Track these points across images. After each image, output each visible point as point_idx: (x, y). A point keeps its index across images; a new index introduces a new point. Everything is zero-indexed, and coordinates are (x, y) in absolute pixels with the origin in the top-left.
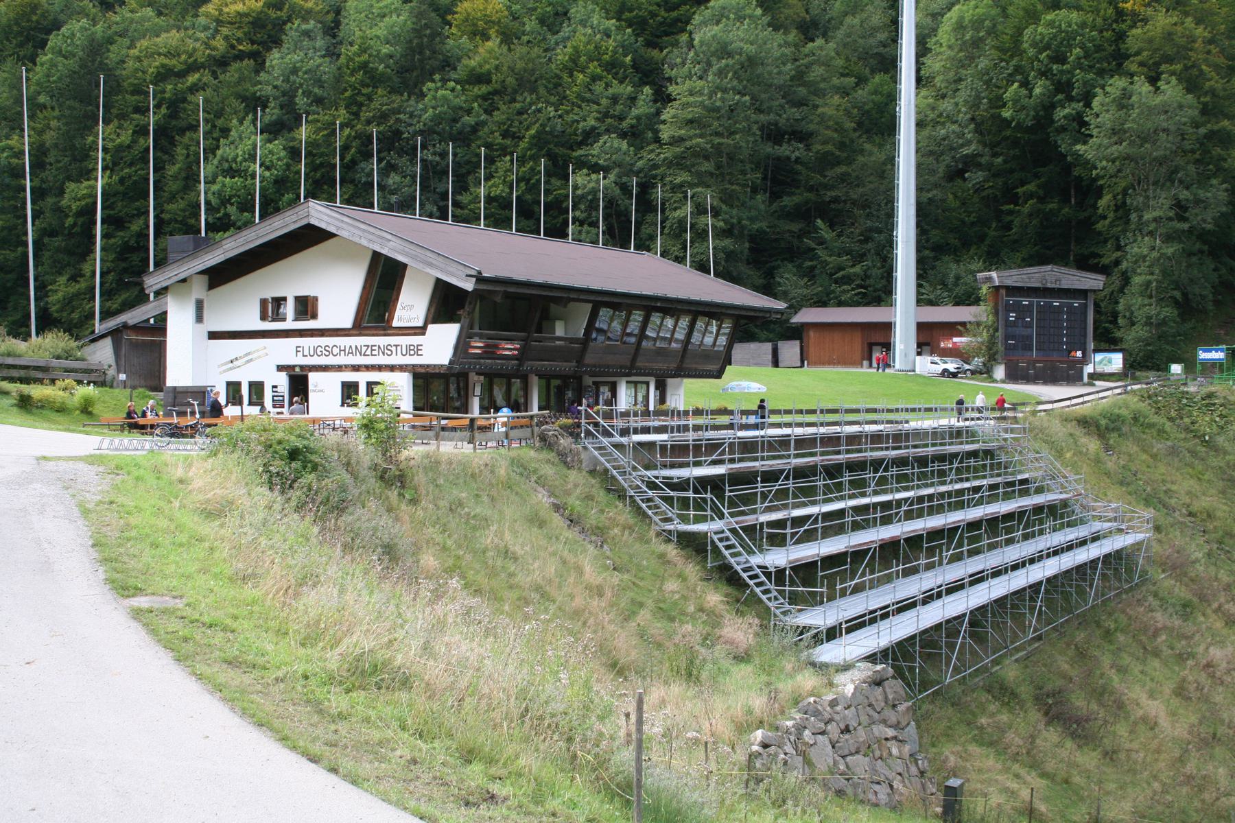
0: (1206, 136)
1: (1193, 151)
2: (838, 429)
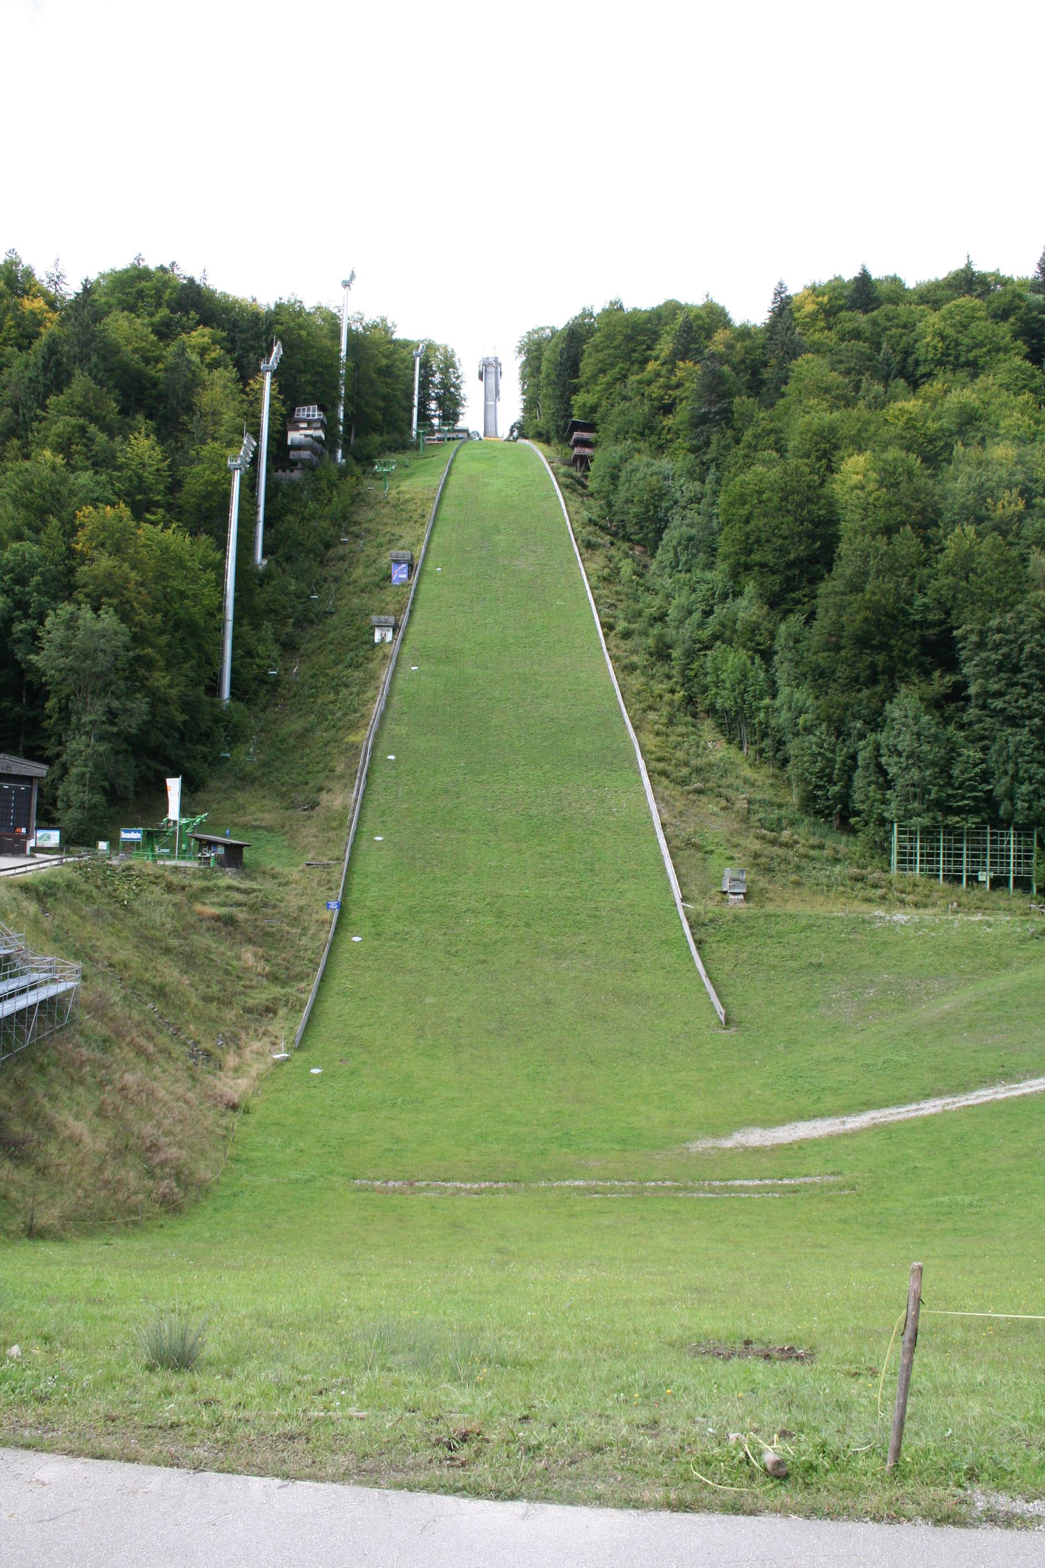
0: (134, 658)
1: (124, 670)
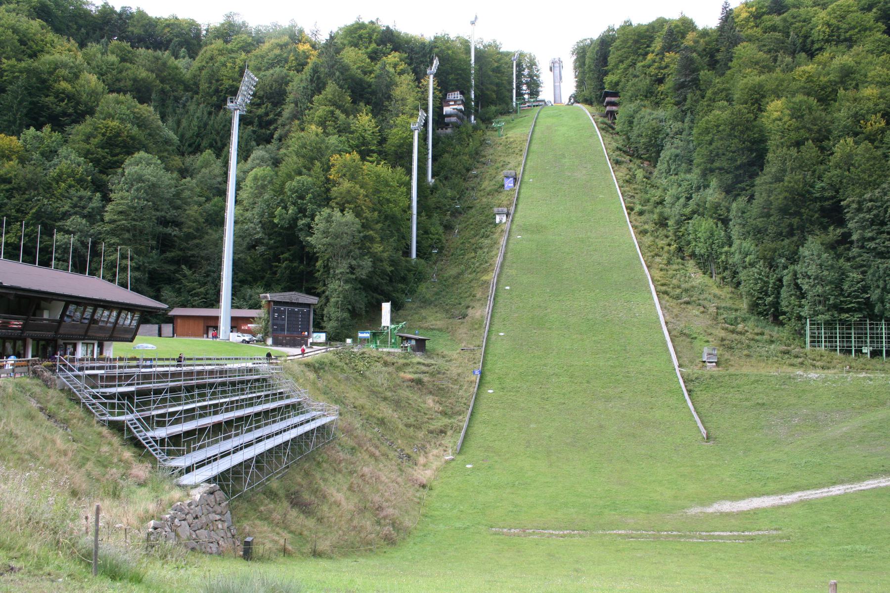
2: (192, 368)
